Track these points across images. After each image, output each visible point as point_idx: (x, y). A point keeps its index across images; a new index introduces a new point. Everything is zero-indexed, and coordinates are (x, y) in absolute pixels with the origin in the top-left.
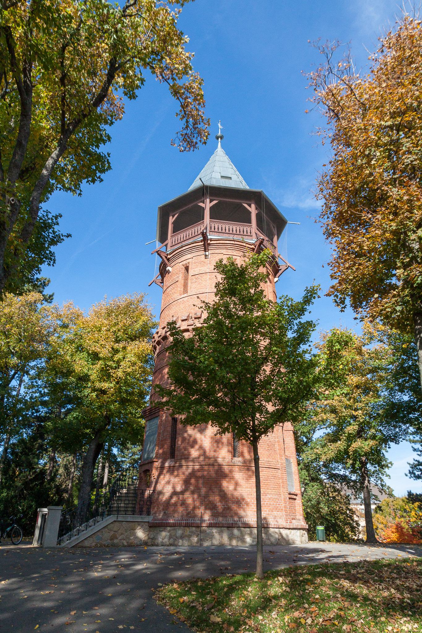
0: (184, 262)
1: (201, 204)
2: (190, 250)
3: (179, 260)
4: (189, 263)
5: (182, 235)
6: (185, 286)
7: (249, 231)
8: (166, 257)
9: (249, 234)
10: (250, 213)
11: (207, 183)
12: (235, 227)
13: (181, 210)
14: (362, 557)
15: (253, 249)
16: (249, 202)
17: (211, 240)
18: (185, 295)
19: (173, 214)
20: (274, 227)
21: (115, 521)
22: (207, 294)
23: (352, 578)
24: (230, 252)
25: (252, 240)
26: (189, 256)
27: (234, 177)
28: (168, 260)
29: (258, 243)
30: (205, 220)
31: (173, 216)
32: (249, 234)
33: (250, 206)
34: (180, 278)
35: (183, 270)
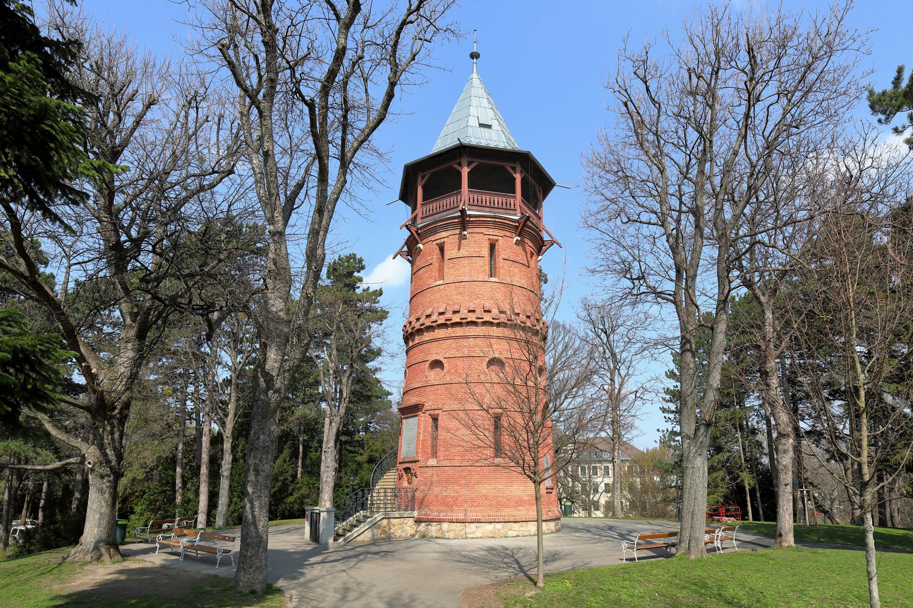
0: (439, 242)
1: (456, 166)
2: (446, 227)
3: (432, 238)
4: (444, 242)
5: (434, 206)
6: (441, 270)
7: (512, 204)
8: (416, 232)
9: (512, 207)
10: (515, 179)
11: (465, 141)
12: (498, 199)
13: (432, 171)
14: (420, 344)
15: (517, 227)
16: (513, 165)
17: (470, 216)
18: (441, 282)
19: (423, 174)
20: (539, 191)
21: (383, 518)
22: (466, 284)
23: (696, 255)
24: (491, 232)
25: (515, 215)
26: (444, 234)
27: (495, 125)
28: (418, 234)
29: (523, 221)
30: (462, 190)
31: (423, 177)
32: (512, 207)
33: (514, 169)
34: (435, 260)
35: (437, 251)
